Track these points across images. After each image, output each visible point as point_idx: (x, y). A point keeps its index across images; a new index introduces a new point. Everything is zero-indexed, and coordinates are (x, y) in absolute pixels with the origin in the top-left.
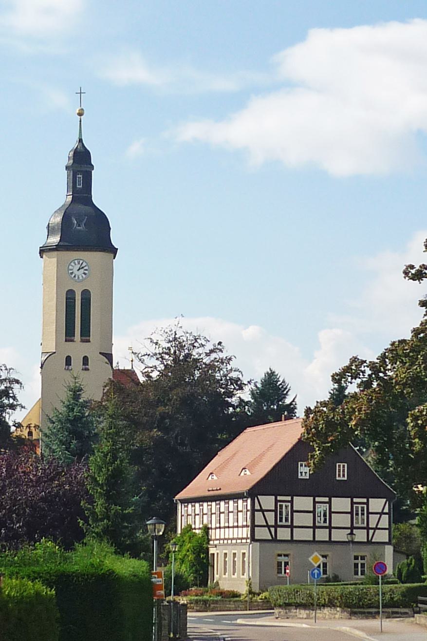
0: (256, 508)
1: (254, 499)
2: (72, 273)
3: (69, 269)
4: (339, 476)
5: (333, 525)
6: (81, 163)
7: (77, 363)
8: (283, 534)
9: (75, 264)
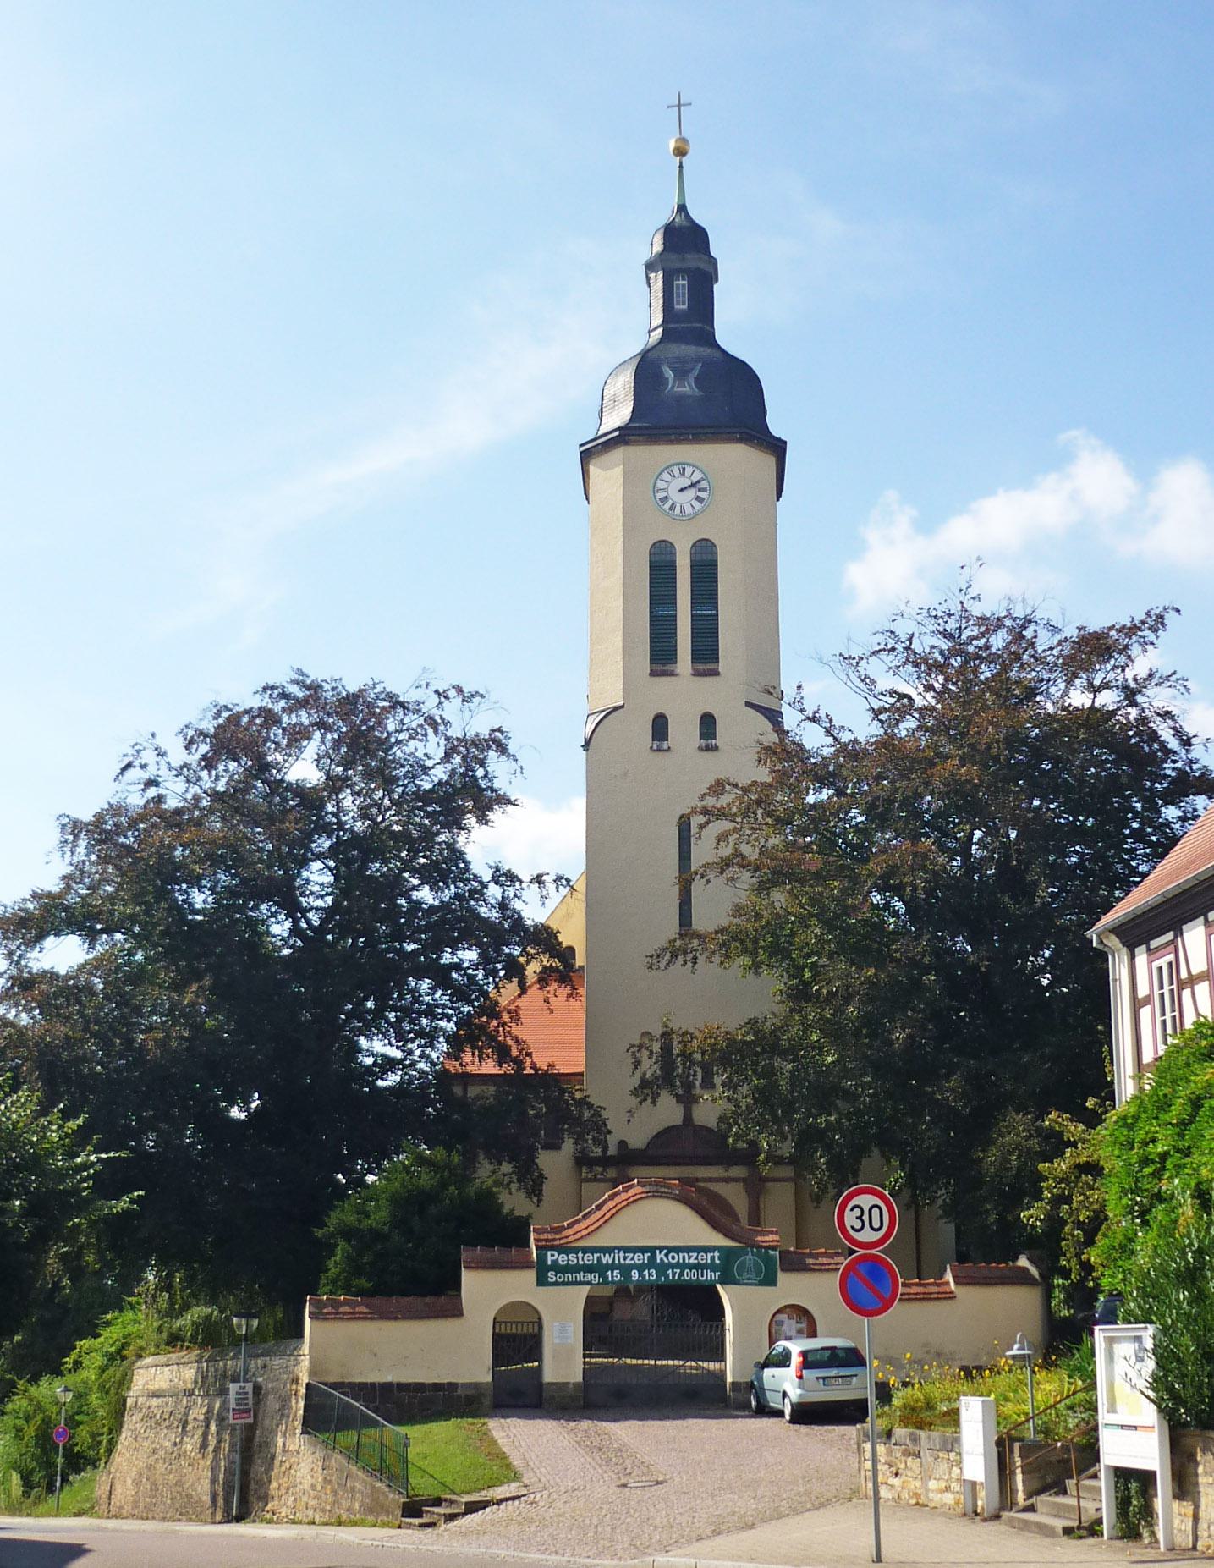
3: (655, 490)
6: (685, 255)
7: (684, 732)
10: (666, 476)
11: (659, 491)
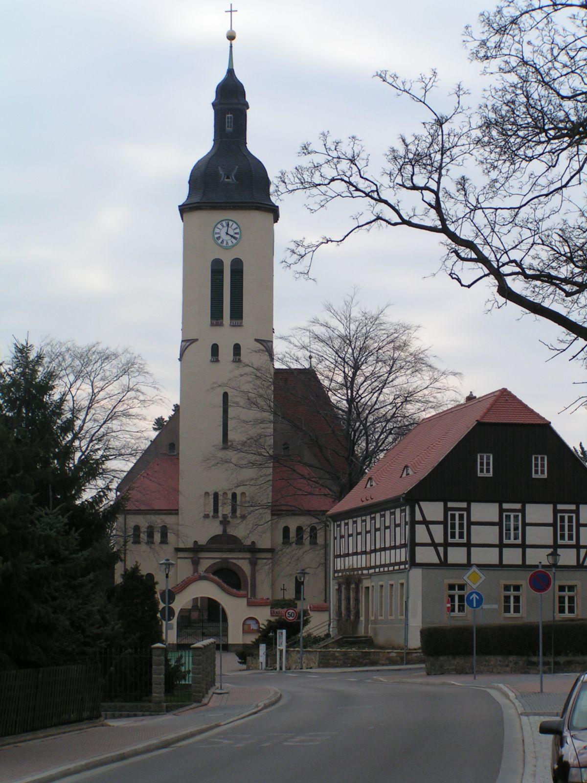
0: (417, 519)
1: (415, 506)
2: (219, 238)
4: (536, 472)
5: (528, 543)
7: (226, 353)
8: (457, 555)
9: (223, 226)
10: (219, 226)
11: (216, 233)
